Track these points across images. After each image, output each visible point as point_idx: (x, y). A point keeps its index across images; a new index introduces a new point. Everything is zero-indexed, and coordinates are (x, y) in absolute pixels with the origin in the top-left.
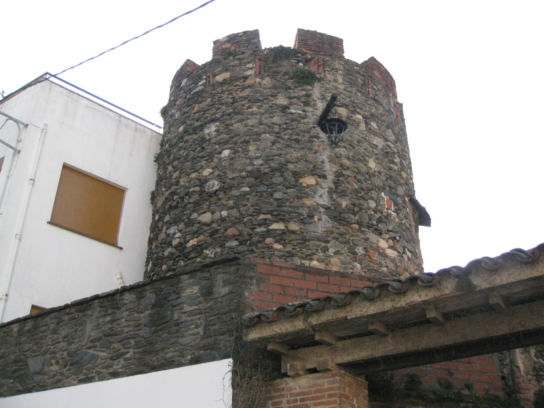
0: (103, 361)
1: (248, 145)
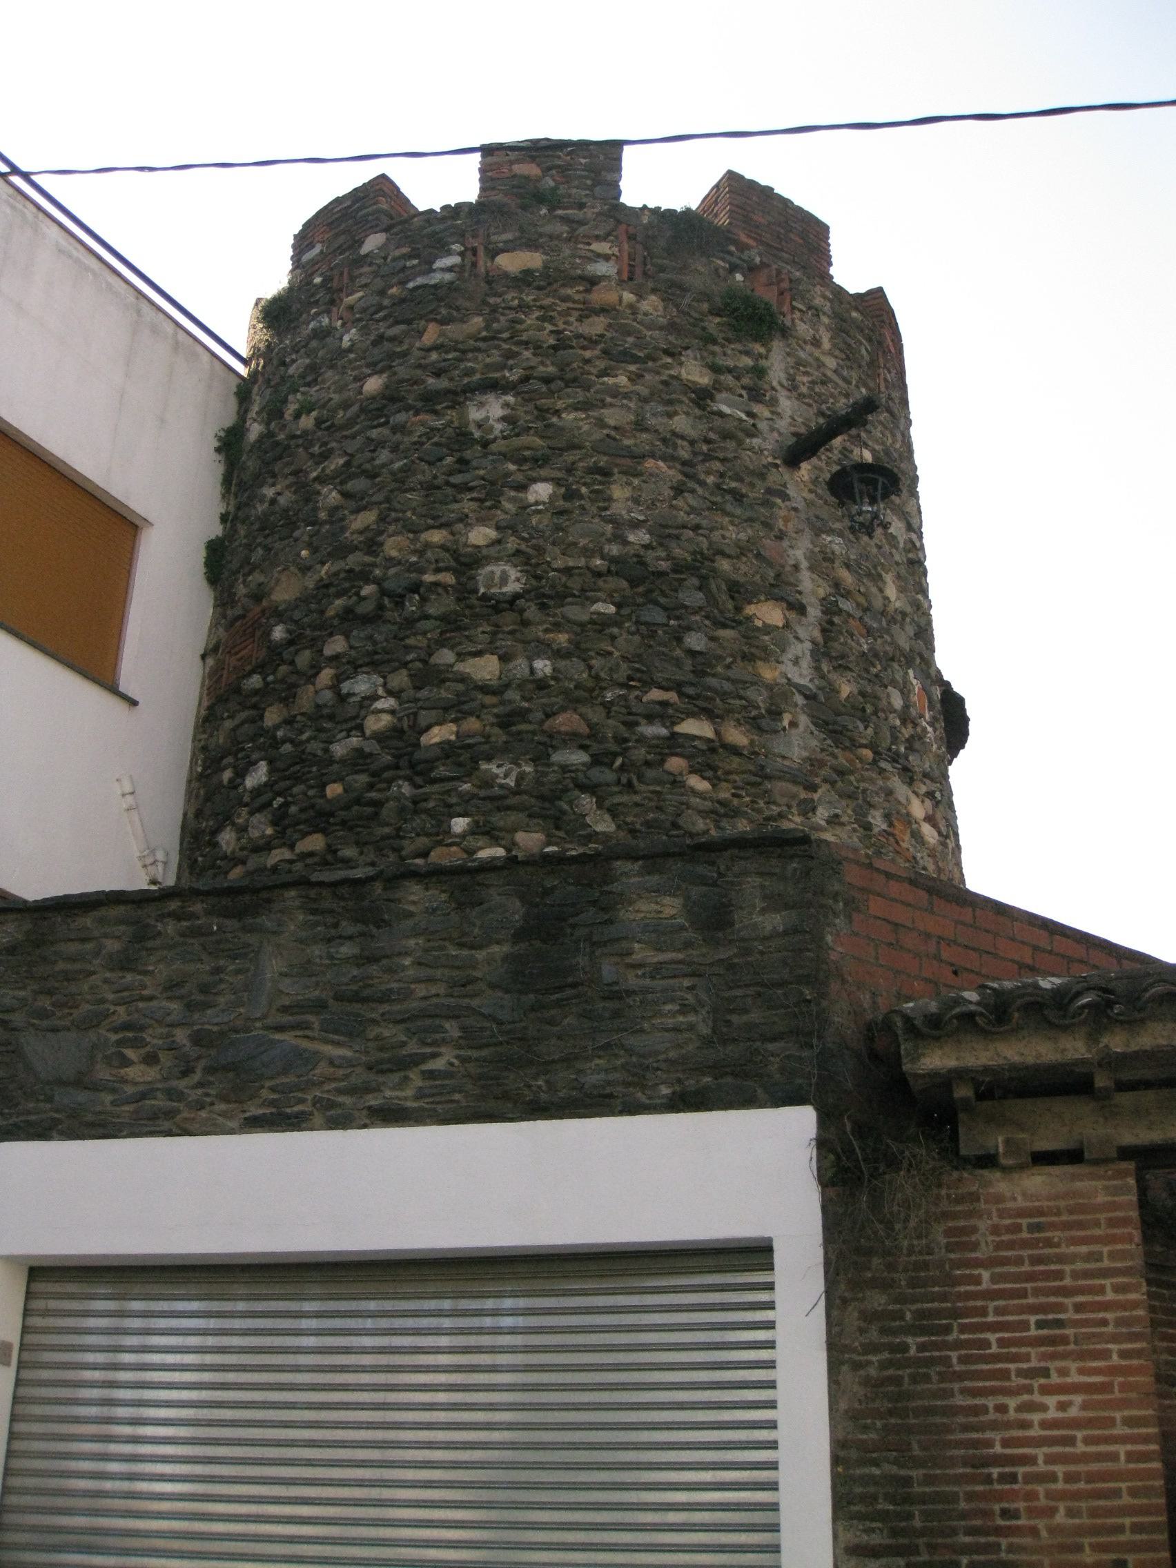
0: (341, 1072)
1: (609, 483)
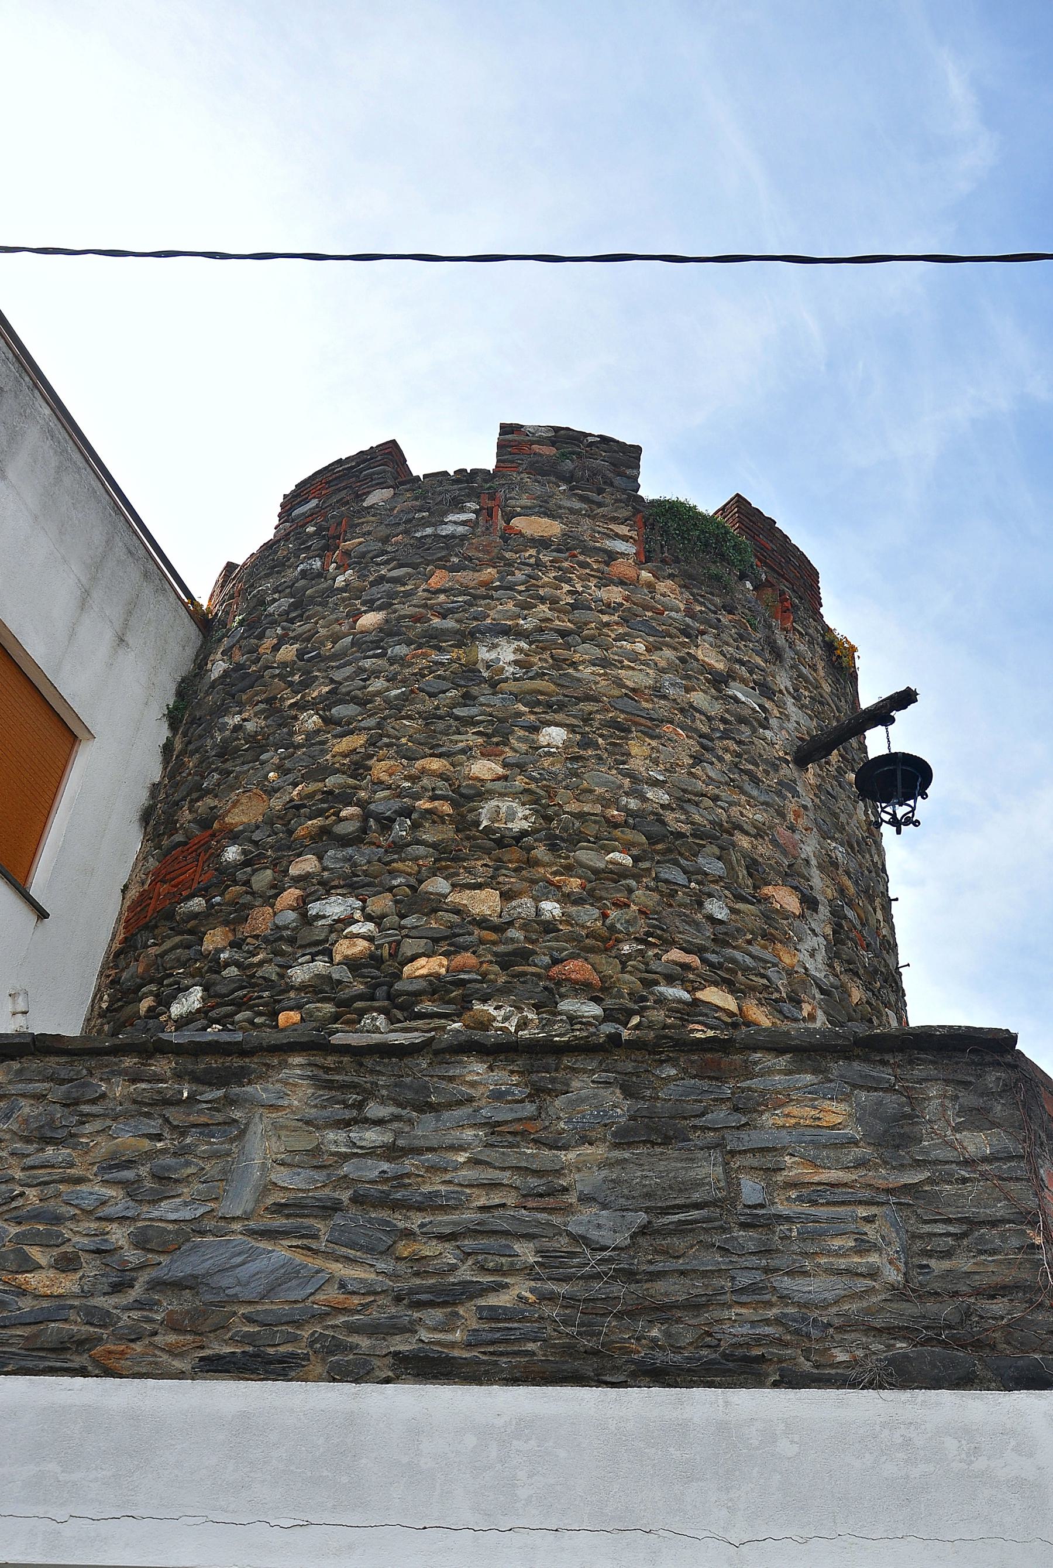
0: (356, 1300)
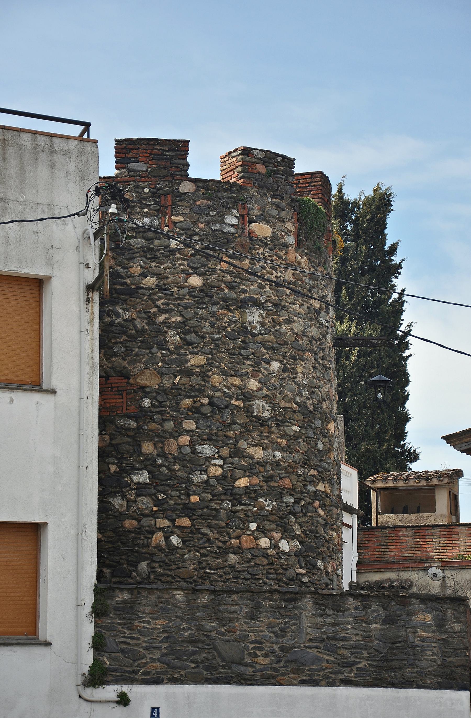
0: (331, 666)
